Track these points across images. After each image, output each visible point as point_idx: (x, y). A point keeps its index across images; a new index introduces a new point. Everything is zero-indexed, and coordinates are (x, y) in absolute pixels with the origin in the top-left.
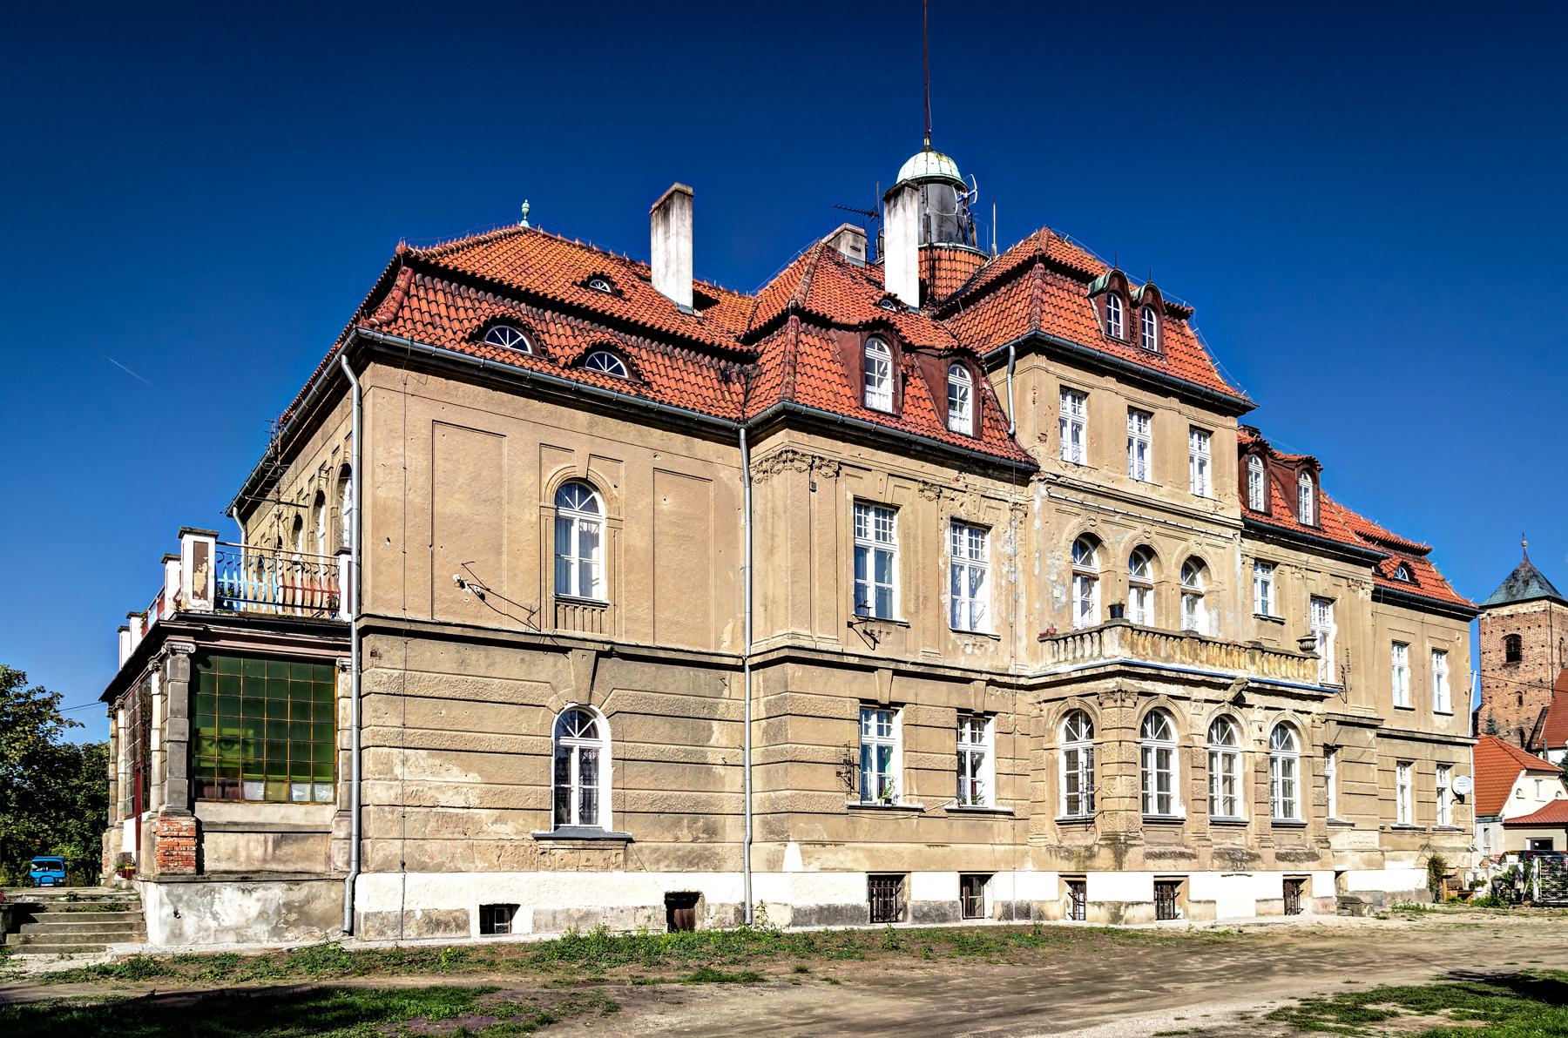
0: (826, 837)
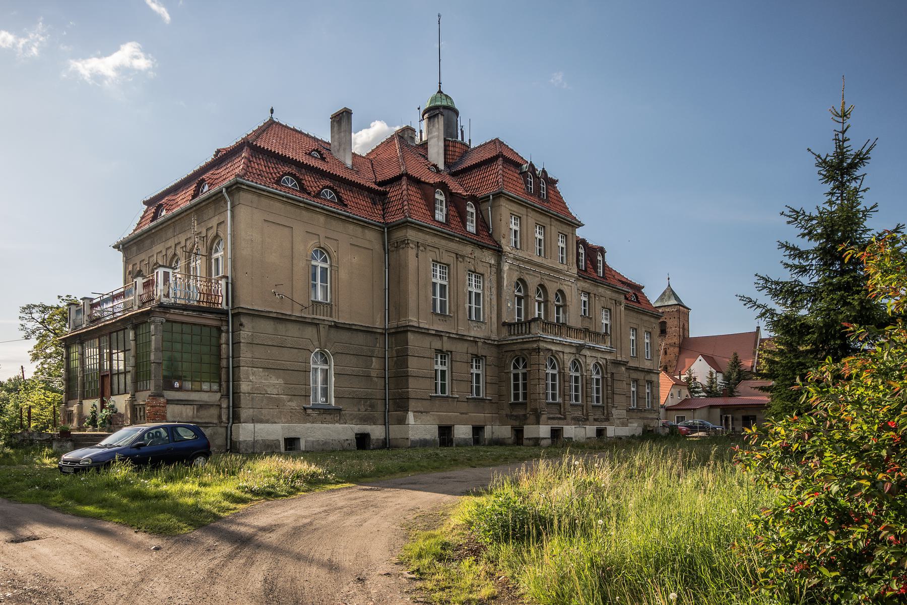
0: (422, 410)
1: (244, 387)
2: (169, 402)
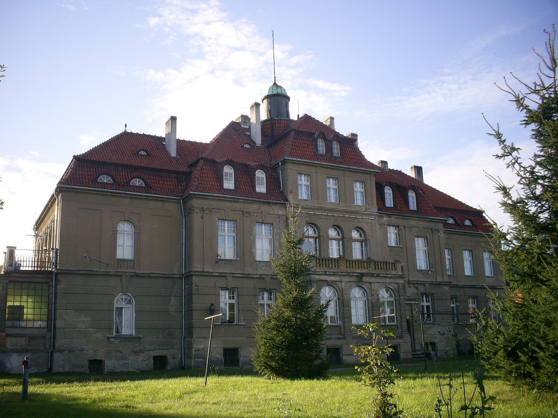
1: (59, 324)
2: (8, 335)
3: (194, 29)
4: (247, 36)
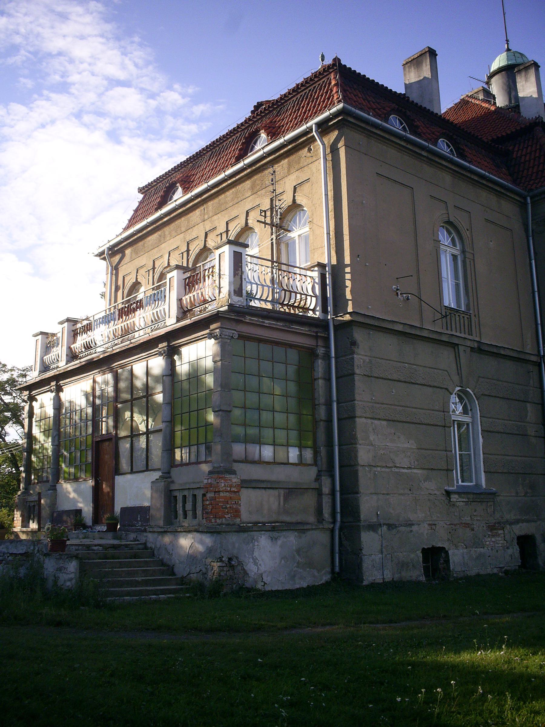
1: (364, 455)
2: (247, 484)
3: (55, 44)
4: (136, 65)
